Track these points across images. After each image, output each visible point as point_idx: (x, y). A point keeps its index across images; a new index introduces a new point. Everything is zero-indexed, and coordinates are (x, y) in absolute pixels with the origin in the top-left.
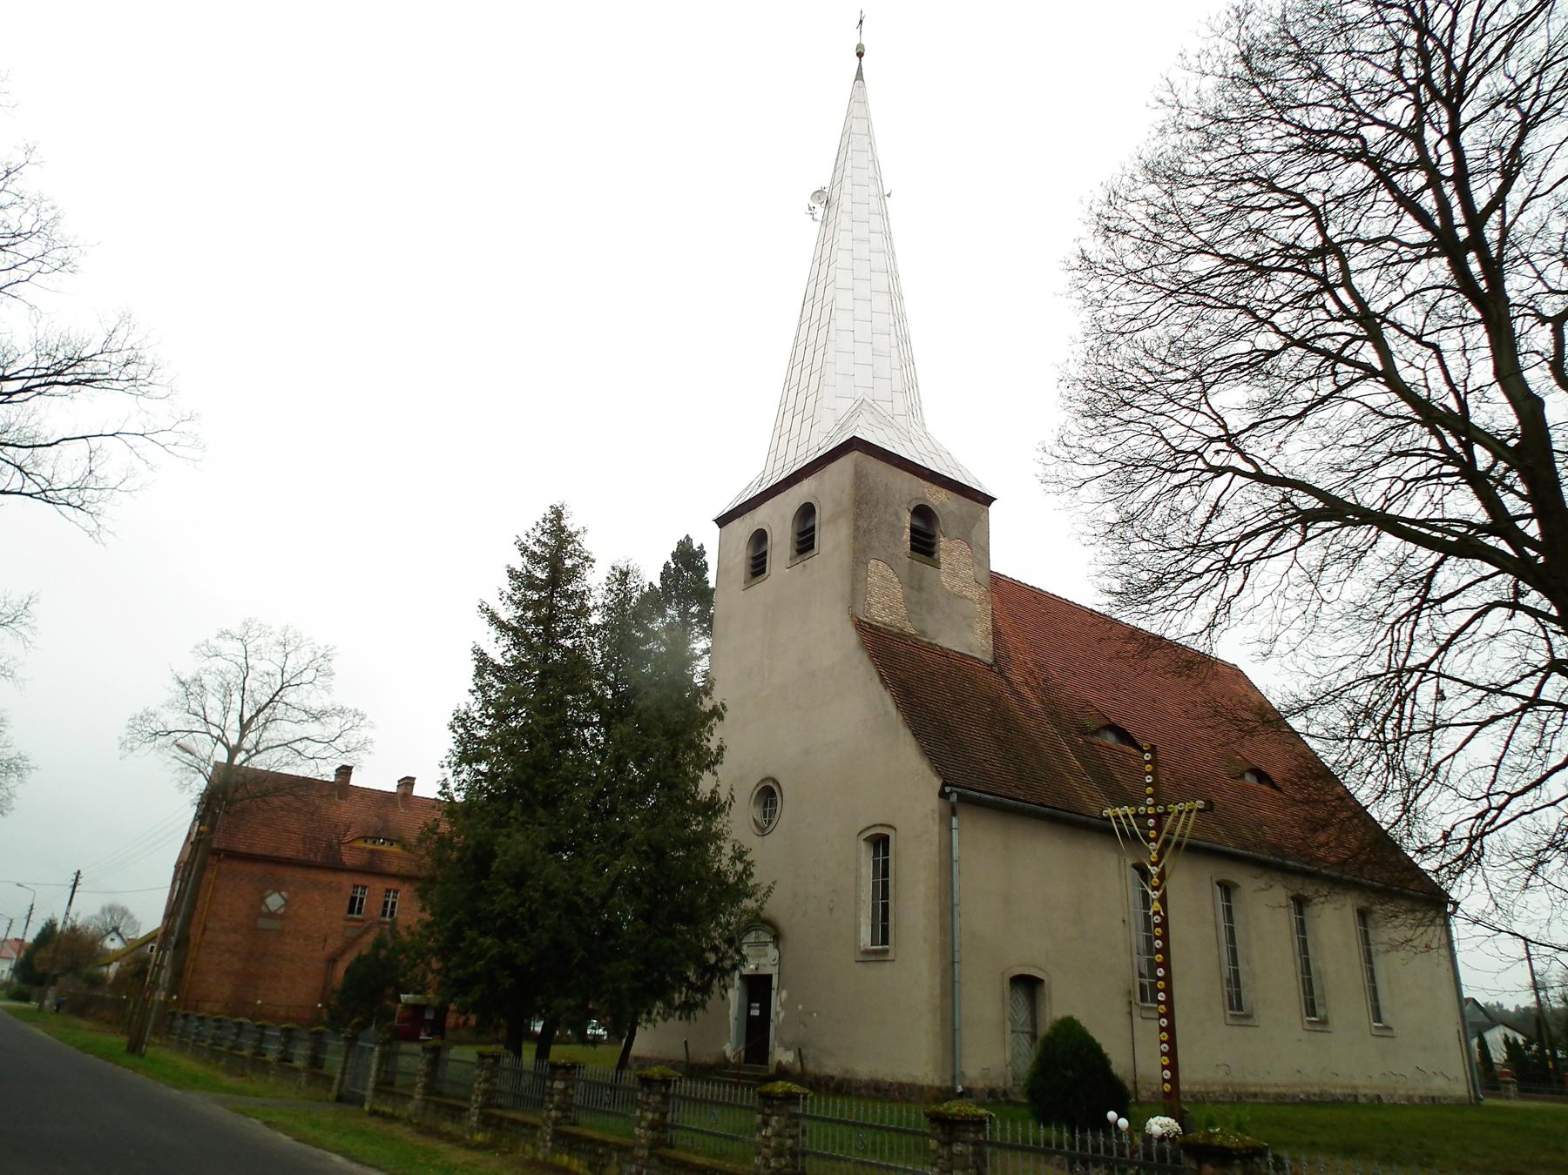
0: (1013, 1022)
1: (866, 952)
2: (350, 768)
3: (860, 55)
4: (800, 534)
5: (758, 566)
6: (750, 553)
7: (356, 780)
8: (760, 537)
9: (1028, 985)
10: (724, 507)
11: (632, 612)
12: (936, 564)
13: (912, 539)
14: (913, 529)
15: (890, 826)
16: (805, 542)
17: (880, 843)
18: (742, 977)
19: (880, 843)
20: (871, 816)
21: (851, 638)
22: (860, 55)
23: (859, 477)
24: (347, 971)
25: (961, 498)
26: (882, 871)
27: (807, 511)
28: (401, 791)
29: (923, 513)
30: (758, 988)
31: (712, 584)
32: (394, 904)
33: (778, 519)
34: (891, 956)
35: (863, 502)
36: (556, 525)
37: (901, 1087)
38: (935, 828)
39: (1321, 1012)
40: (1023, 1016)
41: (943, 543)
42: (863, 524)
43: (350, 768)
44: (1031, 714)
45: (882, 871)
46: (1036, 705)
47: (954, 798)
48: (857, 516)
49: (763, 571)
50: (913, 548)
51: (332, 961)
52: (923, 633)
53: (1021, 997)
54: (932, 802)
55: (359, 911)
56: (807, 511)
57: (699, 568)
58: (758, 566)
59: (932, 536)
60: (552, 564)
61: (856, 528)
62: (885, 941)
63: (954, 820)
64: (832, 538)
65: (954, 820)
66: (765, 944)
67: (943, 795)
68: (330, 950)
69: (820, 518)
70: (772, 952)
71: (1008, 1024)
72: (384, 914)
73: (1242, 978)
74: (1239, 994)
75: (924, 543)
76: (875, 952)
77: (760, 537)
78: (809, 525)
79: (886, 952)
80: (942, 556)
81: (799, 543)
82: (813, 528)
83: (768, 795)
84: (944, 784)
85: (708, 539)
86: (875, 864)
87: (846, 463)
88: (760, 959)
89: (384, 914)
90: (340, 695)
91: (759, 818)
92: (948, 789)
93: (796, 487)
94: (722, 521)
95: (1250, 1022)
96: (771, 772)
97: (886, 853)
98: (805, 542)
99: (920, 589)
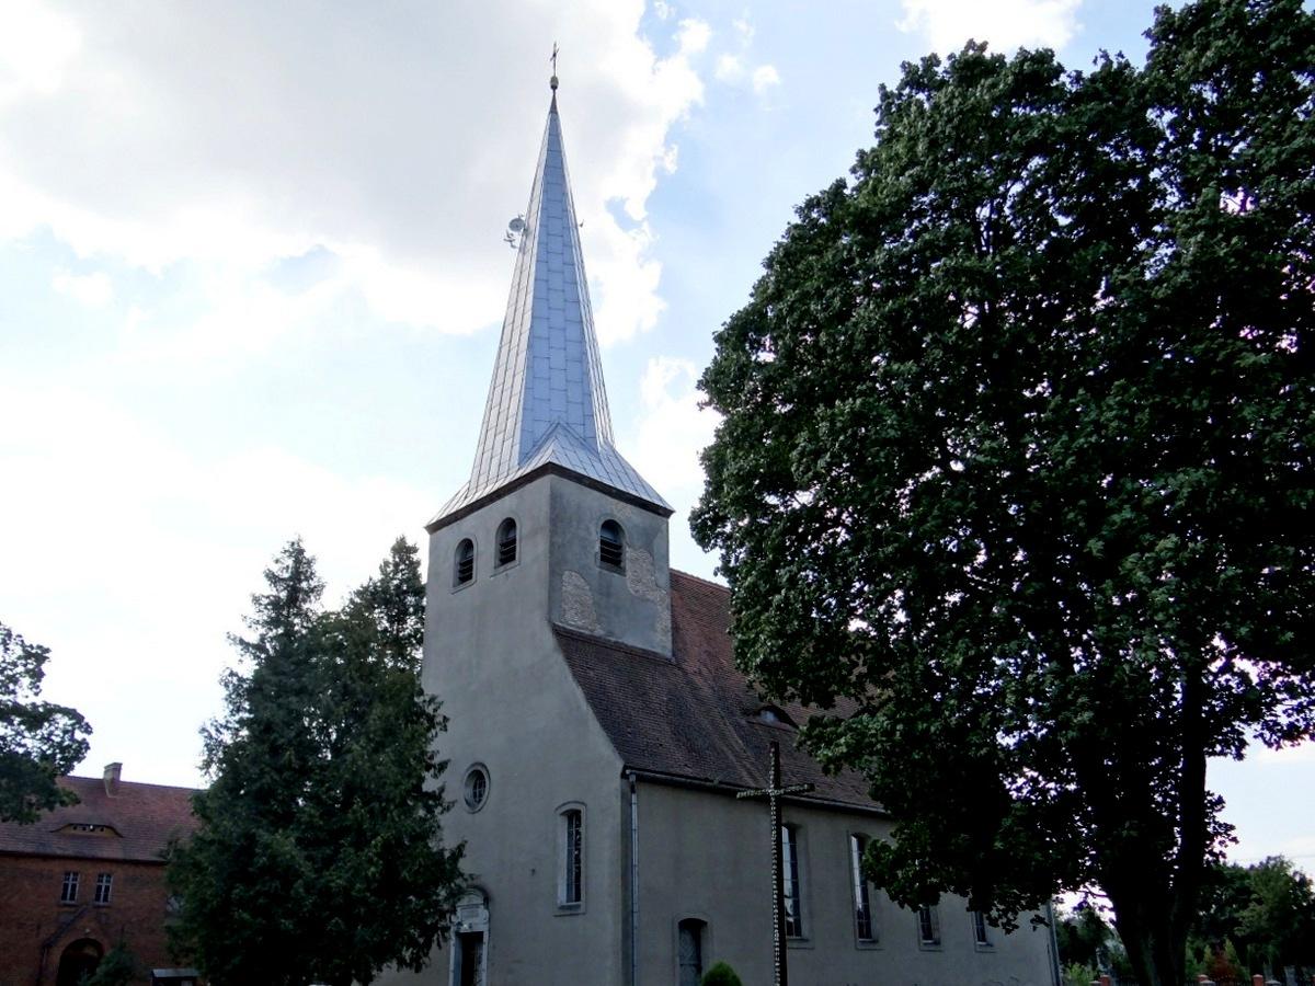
0: (682, 957)
1: (562, 908)
2: (120, 765)
3: (554, 87)
4: (503, 545)
5: (465, 572)
6: (458, 559)
7: (125, 777)
8: (467, 545)
9: (693, 929)
10: (435, 513)
11: (356, 622)
12: (622, 571)
13: (602, 550)
14: (602, 542)
15: (583, 803)
16: (507, 553)
17: (574, 817)
18: (458, 934)
19: (574, 817)
20: (566, 796)
21: (549, 640)
22: (554, 87)
23: (555, 498)
24: (62, 958)
25: (644, 511)
26: (575, 842)
27: (509, 525)
28: (109, 776)
29: (611, 526)
30: (470, 942)
31: (424, 580)
32: (107, 888)
33: (483, 531)
34: (581, 910)
35: (558, 517)
36: (297, 553)
37: (631, 504)
38: (617, 803)
39: (936, 935)
40: (690, 952)
41: (628, 553)
42: (559, 540)
43: (120, 765)
44: (700, 701)
45: (575, 842)
46: (706, 691)
47: (633, 778)
48: (553, 533)
49: (470, 577)
50: (603, 558)
51: (47, 946)
52: (611, 633)
53: (688, 937)
54: (616, 783)
55: (72, 898)
56: (509, 525)
57: (412, 563)
58: (465, 572)
59: (620, 547)
60: (296, 581)
61: (552, 544)
62: (578, 898)
63: (634, 797)
64: (532, 549)
65: (634, 797)
66: (477, 906)
67: (624, 776)
68: (43, 936)
69: (520, 532)
70: (483, 913)
71: (678, 959)
72: (98, 898)
73: (872, 912)
74: (868, 924)
75: (612, 555)
76: (570, 908)
77: (467, 545)
78: (511, 536)
79: (579, 906)
80: (627, 565)
81: (502, 553)
82: (514, 541)
83: (478, 778)
84: (625, 768)
85: (422, 542)
86: (570, 835)
87: (546, 481)
88: (470, 917)
89: (98, 898)
90: (53, 691)
91: (471, 799)
92: (628, 772)
93: (499, 502)
94: (434, 528)
95: (876, 947)
96: (480, 758)
97: (578, 826)
98: (507, 553)
99: (609, 595)
